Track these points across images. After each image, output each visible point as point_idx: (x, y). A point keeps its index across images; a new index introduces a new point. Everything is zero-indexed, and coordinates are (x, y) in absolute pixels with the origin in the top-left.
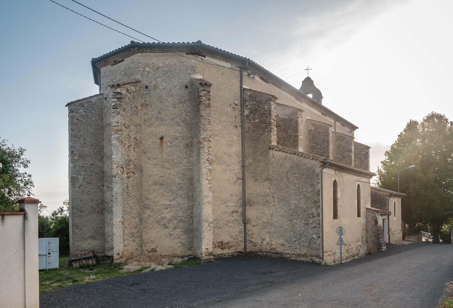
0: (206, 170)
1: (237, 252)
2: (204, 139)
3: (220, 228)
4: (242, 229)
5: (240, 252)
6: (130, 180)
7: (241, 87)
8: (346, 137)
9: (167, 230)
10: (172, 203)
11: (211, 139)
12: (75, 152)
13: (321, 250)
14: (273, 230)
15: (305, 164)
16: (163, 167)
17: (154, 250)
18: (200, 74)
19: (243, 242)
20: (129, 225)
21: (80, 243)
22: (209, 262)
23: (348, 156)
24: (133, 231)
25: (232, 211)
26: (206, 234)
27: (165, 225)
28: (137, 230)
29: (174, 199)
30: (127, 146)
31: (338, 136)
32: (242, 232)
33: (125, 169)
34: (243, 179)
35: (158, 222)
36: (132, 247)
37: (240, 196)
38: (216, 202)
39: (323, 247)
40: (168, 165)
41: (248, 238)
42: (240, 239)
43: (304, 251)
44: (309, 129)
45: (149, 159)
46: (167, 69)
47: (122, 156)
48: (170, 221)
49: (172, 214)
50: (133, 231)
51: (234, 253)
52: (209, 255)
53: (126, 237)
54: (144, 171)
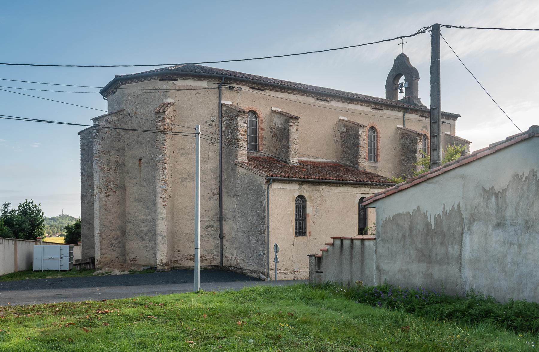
0: (160, 189)
1: (212, 266)
2: (159, 161)
3: (192, 242)
4: (218, 243)
5: (215, 266)
6: (109, 198)
7: (219, 103)
8: (411, 133)
9: (143, 242)
10: (148, 218)
11: (165, 161)
12: (84, 174)
13: (266, 267)
14: (238, 246)
15: (257, 181)
16: (141, 186)
17: (134, 260)
18: (172, 98)
19: (220, 257)
20: (107, 236)
21: (88, 251)
22: (162, 272)
23: (413, 157)
24: (113, 242)
25: (206, 225)
26: (160, 246)
27: (142, 237)
28: (117, 241)
29: (149, 215)
30: (106, 169)
31: (403, 133)
32: (218, 247)
33: (103, 189)
34: (221, 195)
35: (137, 235)
36: (112, 255)
37: (217, 211)
38: (188, 217)
39: (268, 264)
40: (144, 184)
41: (224, 253)
42: (215, 253)
43: (255, 268)
44: (341, 131)
45: (130, 179)
46: (144, 96)
47: (100, 178)
48: (146, 234)
49: (147, 228)
50: (113, 242)
51: (208, 266)
52: (162, 266)
53: (104, 247)
54: (127, 189)
